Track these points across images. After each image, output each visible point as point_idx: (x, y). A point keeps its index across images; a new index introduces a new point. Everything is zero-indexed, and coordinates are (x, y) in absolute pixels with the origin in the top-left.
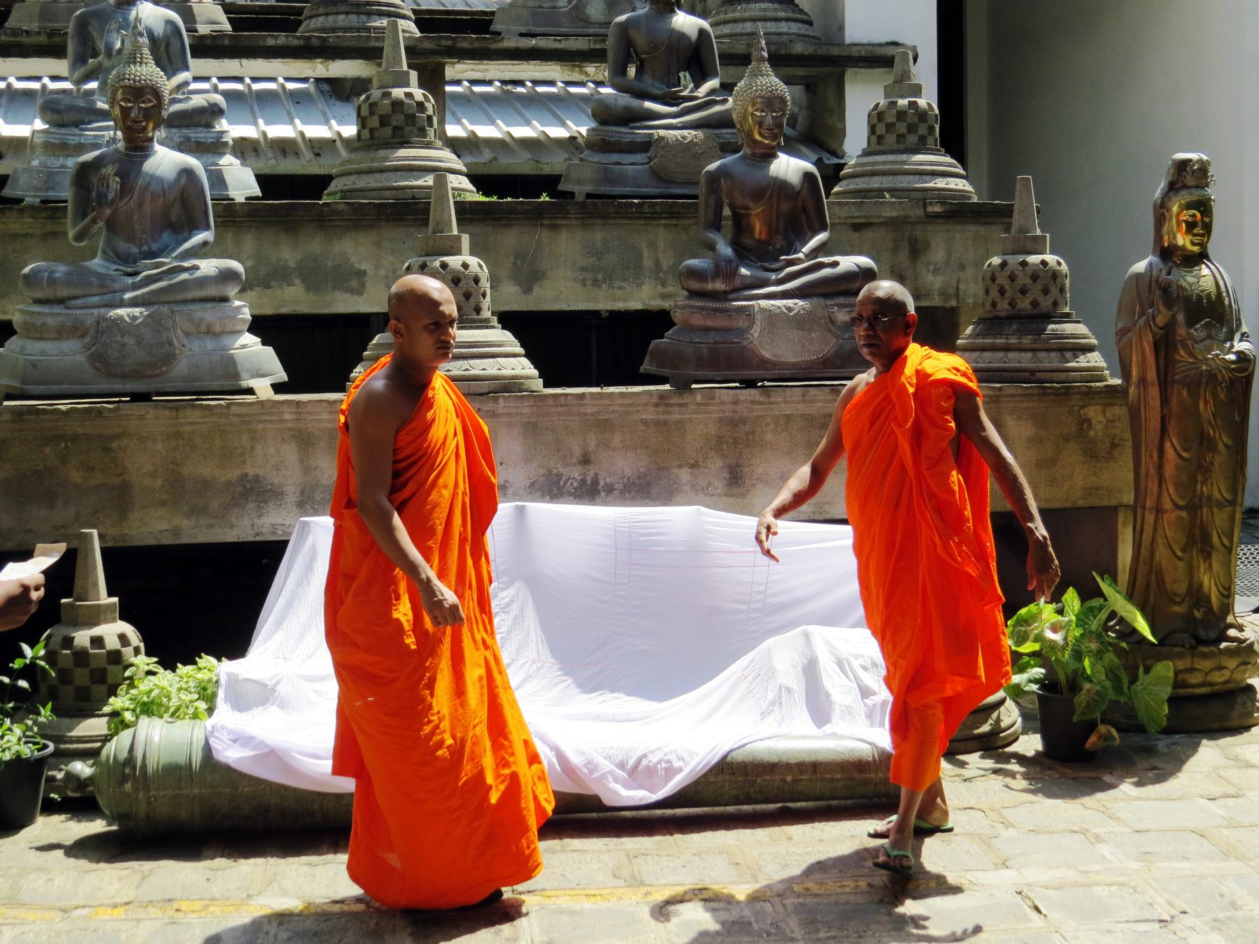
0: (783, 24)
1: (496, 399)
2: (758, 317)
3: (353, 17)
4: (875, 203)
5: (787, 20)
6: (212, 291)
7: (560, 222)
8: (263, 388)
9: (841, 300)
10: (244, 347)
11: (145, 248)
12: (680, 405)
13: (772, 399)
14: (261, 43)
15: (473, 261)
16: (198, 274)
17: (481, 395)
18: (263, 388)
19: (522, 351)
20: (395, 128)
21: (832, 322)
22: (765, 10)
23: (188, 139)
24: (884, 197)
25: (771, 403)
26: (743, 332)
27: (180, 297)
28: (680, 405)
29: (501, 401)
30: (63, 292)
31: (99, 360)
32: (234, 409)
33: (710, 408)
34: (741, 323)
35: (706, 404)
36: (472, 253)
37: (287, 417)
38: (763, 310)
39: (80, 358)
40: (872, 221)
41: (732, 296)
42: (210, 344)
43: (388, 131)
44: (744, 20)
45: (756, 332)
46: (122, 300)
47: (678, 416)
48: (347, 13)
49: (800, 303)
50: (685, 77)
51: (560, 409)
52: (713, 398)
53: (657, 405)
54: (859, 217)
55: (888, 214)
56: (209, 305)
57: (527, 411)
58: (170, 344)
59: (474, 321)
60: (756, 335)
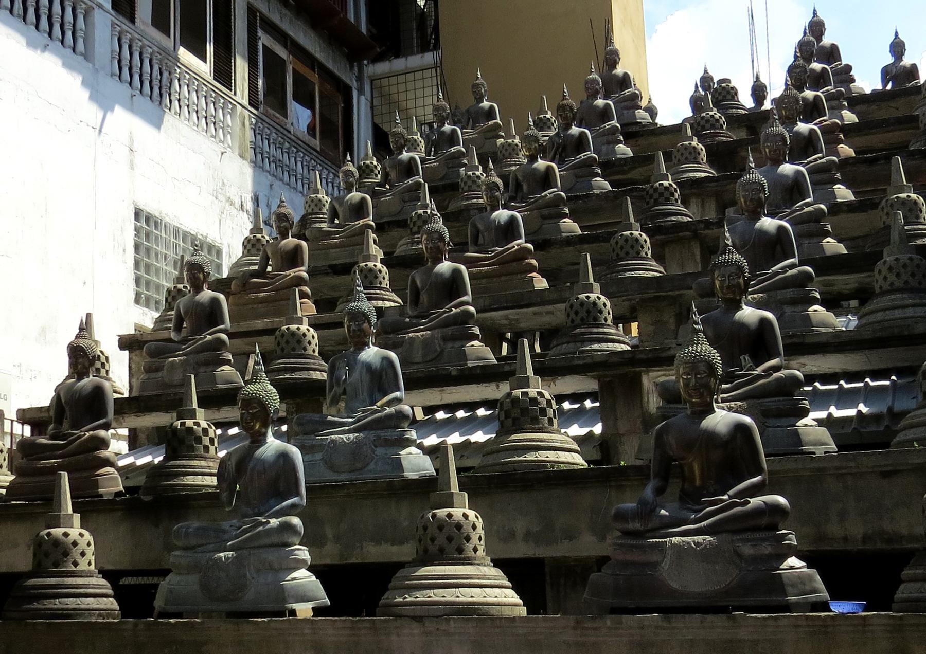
0: (911, 309)
1: (448, 621)
2: (669, 552)
3: (572, 345)
4: (901, 452)
5: (913, 306)
6: (275, 539)
7: (624, 483)
8: (304, 610)
9: (748, 535)
10: (792, 568)
11: (256, 510)
12: (595, 629)
13: (674, 625)
14: (501, 370)
15: (472, 514)
16: (268, 526)
17: (438, 617)
18: (304, 610)
19: (509, 584)
20: (514, 420)
21: (739, 555)
22: (893, 300)
23: (379, 437)
24: (913, 446)
25: (674, 628)
26: (655, 565)
27: (256, 544)
28: (595, 629)
29: (452, 622)
30: (193, 542)
31: (204, 586)
32: (272, 625)
33: (621, 631)
34: (655, 558)
35: (616, 629)
36: (469, 508)
37: (306, 631)
38: (674, 546)
39: (196, 587)
40: (898, 468)
41: (648, 535)
42: (270, 578)
43: (510, 421)
44: (877, 311)
45: (666, 564)
46: (226, 546)
47: (593, 639)
48: (568, 343)
49: (708, 538)
50: (746, 359)
51: (497, 630)
52: (621, 623)
53: (574, 628)
54: (887, 465)
55: (916, 461)
56: (272, 549)
57: (471, 631)
58: (245, 576)
59: (460, 559)
60: (666, 568)
